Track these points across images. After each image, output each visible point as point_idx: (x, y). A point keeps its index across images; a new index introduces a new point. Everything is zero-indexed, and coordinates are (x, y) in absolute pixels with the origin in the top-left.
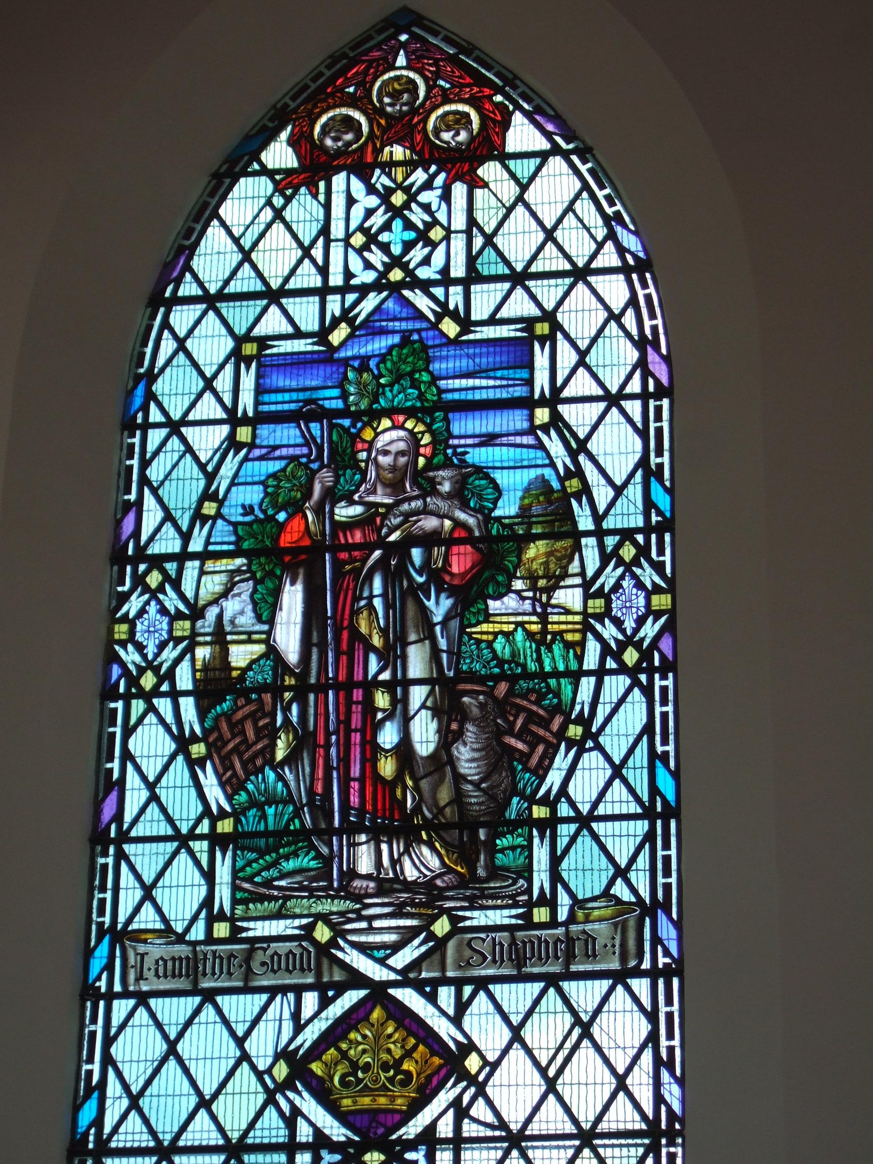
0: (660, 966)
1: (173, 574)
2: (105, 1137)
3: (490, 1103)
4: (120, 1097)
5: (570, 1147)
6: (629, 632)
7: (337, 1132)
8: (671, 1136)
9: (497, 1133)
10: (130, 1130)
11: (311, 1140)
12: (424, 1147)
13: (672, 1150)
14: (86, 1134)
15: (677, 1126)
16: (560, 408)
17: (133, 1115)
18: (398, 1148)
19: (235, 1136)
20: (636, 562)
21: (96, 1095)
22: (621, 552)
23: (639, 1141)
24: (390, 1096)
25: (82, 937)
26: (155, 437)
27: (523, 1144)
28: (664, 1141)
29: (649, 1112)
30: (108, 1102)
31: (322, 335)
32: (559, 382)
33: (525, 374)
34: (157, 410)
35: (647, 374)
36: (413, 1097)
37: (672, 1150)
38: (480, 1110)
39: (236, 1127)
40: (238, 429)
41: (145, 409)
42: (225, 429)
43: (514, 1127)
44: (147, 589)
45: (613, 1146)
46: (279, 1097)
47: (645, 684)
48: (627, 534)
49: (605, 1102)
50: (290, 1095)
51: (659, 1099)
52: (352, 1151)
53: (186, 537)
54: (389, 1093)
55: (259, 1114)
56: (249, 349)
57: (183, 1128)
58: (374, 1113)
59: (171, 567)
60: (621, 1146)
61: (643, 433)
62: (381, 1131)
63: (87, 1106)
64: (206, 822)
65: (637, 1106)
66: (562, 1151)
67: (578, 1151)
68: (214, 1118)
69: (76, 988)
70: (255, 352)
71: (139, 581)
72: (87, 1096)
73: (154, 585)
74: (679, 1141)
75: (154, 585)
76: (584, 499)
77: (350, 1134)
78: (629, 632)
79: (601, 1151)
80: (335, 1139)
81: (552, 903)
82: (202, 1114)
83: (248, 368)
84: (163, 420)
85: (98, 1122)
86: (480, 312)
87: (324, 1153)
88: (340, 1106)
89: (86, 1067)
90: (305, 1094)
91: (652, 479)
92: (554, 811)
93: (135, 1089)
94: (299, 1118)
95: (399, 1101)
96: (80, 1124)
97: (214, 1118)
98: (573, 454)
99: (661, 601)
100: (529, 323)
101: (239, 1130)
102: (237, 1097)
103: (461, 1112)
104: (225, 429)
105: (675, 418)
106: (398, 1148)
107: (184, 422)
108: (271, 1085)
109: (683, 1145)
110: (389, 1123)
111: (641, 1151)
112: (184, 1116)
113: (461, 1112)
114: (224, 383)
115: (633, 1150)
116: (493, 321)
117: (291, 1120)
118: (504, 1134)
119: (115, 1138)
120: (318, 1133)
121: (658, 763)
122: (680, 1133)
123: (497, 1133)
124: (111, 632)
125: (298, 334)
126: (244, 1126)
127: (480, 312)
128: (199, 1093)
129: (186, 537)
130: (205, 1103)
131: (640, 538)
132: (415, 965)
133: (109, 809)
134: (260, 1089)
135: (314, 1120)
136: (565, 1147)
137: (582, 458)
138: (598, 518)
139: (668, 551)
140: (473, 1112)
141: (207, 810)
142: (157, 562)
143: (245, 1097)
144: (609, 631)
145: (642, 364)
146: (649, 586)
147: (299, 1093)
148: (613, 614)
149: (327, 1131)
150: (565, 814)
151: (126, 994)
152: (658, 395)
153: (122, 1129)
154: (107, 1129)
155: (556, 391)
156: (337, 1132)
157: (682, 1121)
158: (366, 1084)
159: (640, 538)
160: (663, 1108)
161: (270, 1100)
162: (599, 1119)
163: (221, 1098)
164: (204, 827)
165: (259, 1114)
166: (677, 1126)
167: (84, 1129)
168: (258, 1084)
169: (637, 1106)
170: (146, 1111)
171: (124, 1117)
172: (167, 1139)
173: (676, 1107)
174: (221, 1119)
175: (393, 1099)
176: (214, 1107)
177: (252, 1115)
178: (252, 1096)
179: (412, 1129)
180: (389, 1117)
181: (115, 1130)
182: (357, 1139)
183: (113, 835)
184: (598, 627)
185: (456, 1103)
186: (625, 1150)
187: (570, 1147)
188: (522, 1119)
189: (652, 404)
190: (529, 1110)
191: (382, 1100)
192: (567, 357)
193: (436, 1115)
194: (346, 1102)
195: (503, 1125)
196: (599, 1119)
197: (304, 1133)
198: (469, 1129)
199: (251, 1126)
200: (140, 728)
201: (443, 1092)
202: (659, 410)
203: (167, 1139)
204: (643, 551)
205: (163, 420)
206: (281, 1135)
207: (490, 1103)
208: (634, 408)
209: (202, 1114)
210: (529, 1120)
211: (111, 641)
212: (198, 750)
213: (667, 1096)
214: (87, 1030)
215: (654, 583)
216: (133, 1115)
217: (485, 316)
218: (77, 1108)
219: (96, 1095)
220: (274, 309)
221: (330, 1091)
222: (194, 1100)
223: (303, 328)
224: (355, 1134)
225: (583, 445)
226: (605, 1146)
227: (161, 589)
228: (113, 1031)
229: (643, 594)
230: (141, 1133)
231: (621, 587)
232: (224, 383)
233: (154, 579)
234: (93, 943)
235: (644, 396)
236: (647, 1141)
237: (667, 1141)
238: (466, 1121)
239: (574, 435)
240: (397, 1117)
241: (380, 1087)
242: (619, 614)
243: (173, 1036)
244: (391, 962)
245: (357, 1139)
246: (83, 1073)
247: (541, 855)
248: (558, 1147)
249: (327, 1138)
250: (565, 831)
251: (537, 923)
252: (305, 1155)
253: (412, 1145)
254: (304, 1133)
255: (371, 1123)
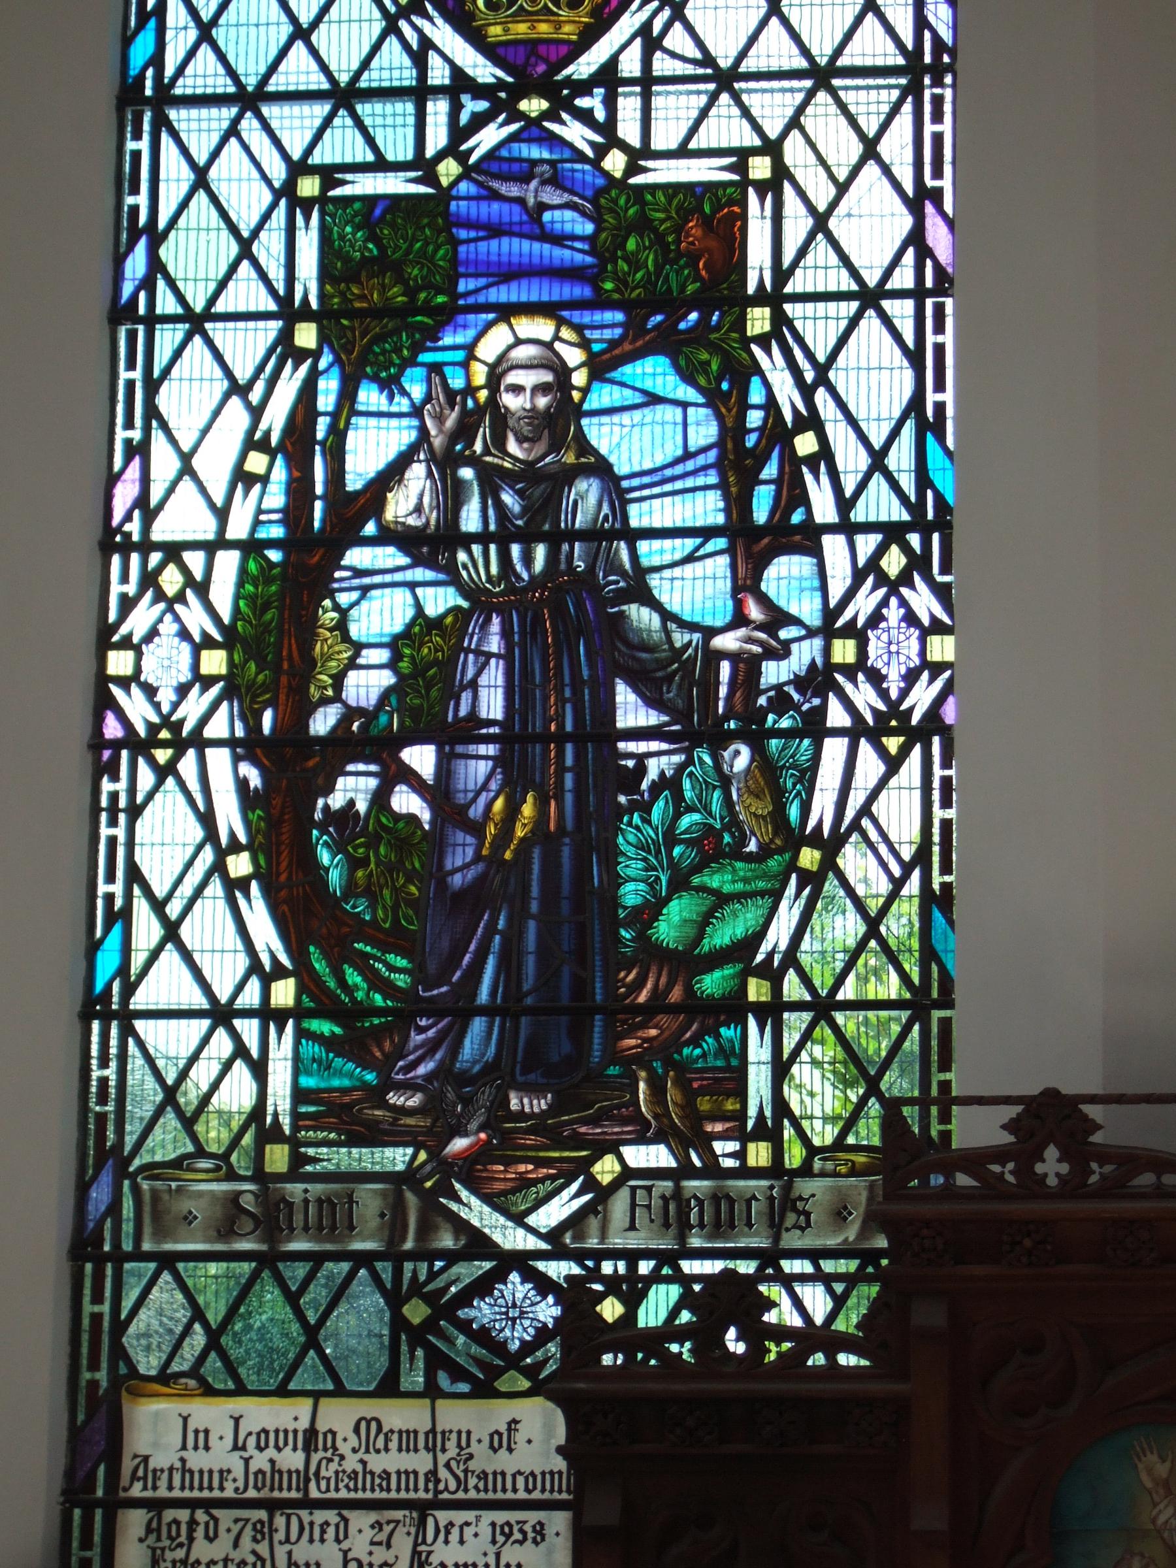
0: (936, 887)
1: (198, 575)
2: (133, 979)
3: (690, 29)
4: (185, 28)
5: (800, 90)
6: (894, 601)
7: (483, 71)
8: (937, 72)
9: (700, 71)
10: (200, 72)
11: (447, 81)
12: (602, 90)
13: (938, 91)
14: (141, 77)
15: (946, 59)
16: (788, 307)
17: (205, 50)
18: (565, 92)
19: (344, 79)
20: (905, 578)
21: (152, 24)
22: (884, 563)
23: (892, 81)
24: (554, 21)
25: (82, 928)
26: (167, 338)
27: (736, 86)
28: (927, 81)
29: (908, 37)
30: (169, 35)
31: (423, 166)
32: (787, 260)
33: (731, 1105)
34: (170, 140)
35: (924, 252)
36: (586, 24)
37: (938, 91)
38: (677, 39)
39: (344, 67)
40: (268, 1148)
41: (148, 284)
42: (275, 325)
43: (724, 63)
44: (160, 596)
45: (858, 88)
46: (403, 25)
47: (918, 552)
48: (892, 533)
49: (846, 29)
50: (418, 21)
51: (921, 23)
52: (503, 95)
53: (222, 514)
54: (552, 18)
55: (376, 48)
56: (309, 187)
57: (273, 68)
58: (532, 45)
59: (195, 560)
60: (868, 88)
61: (915, 357)
62: (541, 68)
63: (140, 39)
64: (254, 985)
65: (890, 30)
66: (788, 95)
67: (811, 94)
68: (314, 52)
69: (73, 1001)
70: (316, 193)
71: (149, 580)
72: (141, 25)
73: (170, 590)
74: (948, 79)
75: (170, 590)
76: (823, 468)
77: (500, 74)
78: (894, 601)
79: (842, 94)
80: (480, 80)
81: (773, 1136)
82: (299, 47)
83: (280, 1032)
84: (180, 311)
85: (157, 60)
86: (665, 137)
87: (465, 98)
88: (486, 36)
89: (130, 200)
90: (439, 21)
91: (929, 435)
92: (777, 989)
93: (206, 15)
94: (430, 52)
95: (567, 28)
96: (132, 67)
97: (314, 52)
98: (807, 392)
99: (942, 648)
100: (743, 155)
101: (349, 71)
102: (345, 26)
103: (651, 43)
104: (275, 325)
105: (958, 100)
106: (565, 92)
107: (208, 315)
108: (392, 9)
109: (954, 86)
110: (553, 58)
111: (895, 94)
112: (273, 53)
113: (651, 43)
114: (270, 247)
115: (884, 92)
116: (683, 152)
117: (420, 56)
118: (709, 71)
119: (180, 82)
120: (457, 73)
121: (930, 437)
122: (950, 68)
123: (700, 71)
124: (102, 662)
125: (381, 165)
126: (355, 65)
127: (665, 137)
128: (293, 19)
129: (222, 514)
130: (302, 33)
131: (914, 539)
132: (575, 1222)
133: (107, 962)
134: (377, 14)
135: (450, 56)
136: (792, 90)
137: (821, 396)
138: (845, 504)
139: (948, 169)
140: (667, 43)
141: (255, 967)
142: (173, 551)
143: (355, 26)
144: (864, 696)
145: (917, 238)
146: (926, 621)
147: (430, 19)
148: (869, 664)
149: (470, 71)
150: (795, 997)
151: (139, 1256)
152: (939, 291)
153: (189, 71)
154: (169, 71)
155: (782, 275)
156: (483, 71)
157: (953, 52)
158: (521, 6)
159: (914, 539)
160: (927, 35)
161: (391, 28)
162: (838, 52)
163: (323, 27)
164: (251, 996)
165: (376, 48)
166: (946, 59)
167: (137, 71)
168: (367, 148)
169: (890, 30)
170: (221, 43)
171: (191, 54)
172: (251, 82)
173: (946, 35)
174: (323, 53)
175: (558, 26)
176: (314, 38)
177: (366, 50)
178: (365, 25)
179: (585, 66)
180: (553, 48)
181: (180, 71)
182: (510, 80)
183: (148, 92)
184: (849, 688)
185: (645, 31)
186: (873, 93)
187: (800, 90)
188: (733, 53)
189: (929, 303)
190: (743, 41)
191: (543, 28)
192: (797, 225)
193: (616, 47)
194: (495, 31)
195: (708, 60)
196: (838, 52)
197: (438, 74)
198: (662, 65)
199: (366, 64)
200: (173, 234)
201: (627, 15)
202: (939, 310)
203: (251, 82)
204: (918, 563)
205: (180, 311)
206: (407, 76)
207: (690, 29)
208: (902, 311)
209: (299, 47)
210: (743, 55)
211: (103, 679)
212: (239, 865)
213: (931, 18)
214: (74, 1559)
215: (934, 619)
216: (205, 50)
217: (673, 145)
218: (127, 41)
219: (152, 24)
220: (343, 119)
221: (472, 16)
222: (287, 29)
223: (390, 157)
224: (509, 74)
225: (822, 370)
226: (846, 88)
227: (181, 598)
228: (137, 891)
229: (917, 632)
230: (216, 75)
231: (884, 619)
232: (270, 247)
233: (171, 580)
234: (99, 933)
235: (918, 294)
236: (903, 81)
237: (932, 79)
238: (658, 54)
239: (810, 355)
240: (564, 50)
241: (541, 9)
242: (879, 665)
243: (245, 264)
244: (531, 1220)
245: (510, 80)
246: (126, 209)
247: (759, 1051)
248: (783, 90)
249: (472, 80)
250: (795, 1023)
251: (753, 1003)
252: (438, 103)
253: (584, 87)
254: (438, 74)
255: (528, 59)
